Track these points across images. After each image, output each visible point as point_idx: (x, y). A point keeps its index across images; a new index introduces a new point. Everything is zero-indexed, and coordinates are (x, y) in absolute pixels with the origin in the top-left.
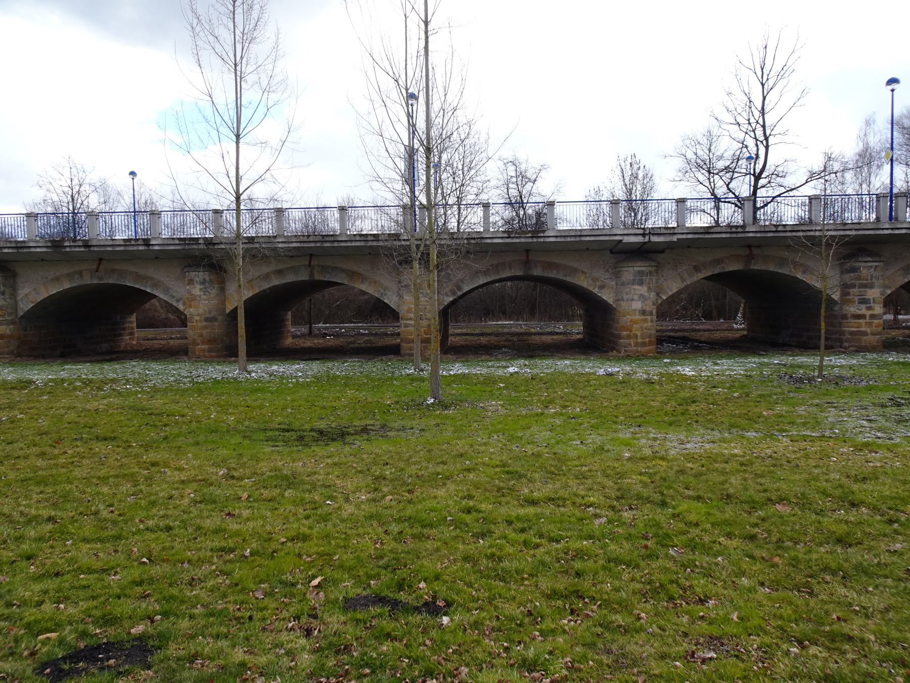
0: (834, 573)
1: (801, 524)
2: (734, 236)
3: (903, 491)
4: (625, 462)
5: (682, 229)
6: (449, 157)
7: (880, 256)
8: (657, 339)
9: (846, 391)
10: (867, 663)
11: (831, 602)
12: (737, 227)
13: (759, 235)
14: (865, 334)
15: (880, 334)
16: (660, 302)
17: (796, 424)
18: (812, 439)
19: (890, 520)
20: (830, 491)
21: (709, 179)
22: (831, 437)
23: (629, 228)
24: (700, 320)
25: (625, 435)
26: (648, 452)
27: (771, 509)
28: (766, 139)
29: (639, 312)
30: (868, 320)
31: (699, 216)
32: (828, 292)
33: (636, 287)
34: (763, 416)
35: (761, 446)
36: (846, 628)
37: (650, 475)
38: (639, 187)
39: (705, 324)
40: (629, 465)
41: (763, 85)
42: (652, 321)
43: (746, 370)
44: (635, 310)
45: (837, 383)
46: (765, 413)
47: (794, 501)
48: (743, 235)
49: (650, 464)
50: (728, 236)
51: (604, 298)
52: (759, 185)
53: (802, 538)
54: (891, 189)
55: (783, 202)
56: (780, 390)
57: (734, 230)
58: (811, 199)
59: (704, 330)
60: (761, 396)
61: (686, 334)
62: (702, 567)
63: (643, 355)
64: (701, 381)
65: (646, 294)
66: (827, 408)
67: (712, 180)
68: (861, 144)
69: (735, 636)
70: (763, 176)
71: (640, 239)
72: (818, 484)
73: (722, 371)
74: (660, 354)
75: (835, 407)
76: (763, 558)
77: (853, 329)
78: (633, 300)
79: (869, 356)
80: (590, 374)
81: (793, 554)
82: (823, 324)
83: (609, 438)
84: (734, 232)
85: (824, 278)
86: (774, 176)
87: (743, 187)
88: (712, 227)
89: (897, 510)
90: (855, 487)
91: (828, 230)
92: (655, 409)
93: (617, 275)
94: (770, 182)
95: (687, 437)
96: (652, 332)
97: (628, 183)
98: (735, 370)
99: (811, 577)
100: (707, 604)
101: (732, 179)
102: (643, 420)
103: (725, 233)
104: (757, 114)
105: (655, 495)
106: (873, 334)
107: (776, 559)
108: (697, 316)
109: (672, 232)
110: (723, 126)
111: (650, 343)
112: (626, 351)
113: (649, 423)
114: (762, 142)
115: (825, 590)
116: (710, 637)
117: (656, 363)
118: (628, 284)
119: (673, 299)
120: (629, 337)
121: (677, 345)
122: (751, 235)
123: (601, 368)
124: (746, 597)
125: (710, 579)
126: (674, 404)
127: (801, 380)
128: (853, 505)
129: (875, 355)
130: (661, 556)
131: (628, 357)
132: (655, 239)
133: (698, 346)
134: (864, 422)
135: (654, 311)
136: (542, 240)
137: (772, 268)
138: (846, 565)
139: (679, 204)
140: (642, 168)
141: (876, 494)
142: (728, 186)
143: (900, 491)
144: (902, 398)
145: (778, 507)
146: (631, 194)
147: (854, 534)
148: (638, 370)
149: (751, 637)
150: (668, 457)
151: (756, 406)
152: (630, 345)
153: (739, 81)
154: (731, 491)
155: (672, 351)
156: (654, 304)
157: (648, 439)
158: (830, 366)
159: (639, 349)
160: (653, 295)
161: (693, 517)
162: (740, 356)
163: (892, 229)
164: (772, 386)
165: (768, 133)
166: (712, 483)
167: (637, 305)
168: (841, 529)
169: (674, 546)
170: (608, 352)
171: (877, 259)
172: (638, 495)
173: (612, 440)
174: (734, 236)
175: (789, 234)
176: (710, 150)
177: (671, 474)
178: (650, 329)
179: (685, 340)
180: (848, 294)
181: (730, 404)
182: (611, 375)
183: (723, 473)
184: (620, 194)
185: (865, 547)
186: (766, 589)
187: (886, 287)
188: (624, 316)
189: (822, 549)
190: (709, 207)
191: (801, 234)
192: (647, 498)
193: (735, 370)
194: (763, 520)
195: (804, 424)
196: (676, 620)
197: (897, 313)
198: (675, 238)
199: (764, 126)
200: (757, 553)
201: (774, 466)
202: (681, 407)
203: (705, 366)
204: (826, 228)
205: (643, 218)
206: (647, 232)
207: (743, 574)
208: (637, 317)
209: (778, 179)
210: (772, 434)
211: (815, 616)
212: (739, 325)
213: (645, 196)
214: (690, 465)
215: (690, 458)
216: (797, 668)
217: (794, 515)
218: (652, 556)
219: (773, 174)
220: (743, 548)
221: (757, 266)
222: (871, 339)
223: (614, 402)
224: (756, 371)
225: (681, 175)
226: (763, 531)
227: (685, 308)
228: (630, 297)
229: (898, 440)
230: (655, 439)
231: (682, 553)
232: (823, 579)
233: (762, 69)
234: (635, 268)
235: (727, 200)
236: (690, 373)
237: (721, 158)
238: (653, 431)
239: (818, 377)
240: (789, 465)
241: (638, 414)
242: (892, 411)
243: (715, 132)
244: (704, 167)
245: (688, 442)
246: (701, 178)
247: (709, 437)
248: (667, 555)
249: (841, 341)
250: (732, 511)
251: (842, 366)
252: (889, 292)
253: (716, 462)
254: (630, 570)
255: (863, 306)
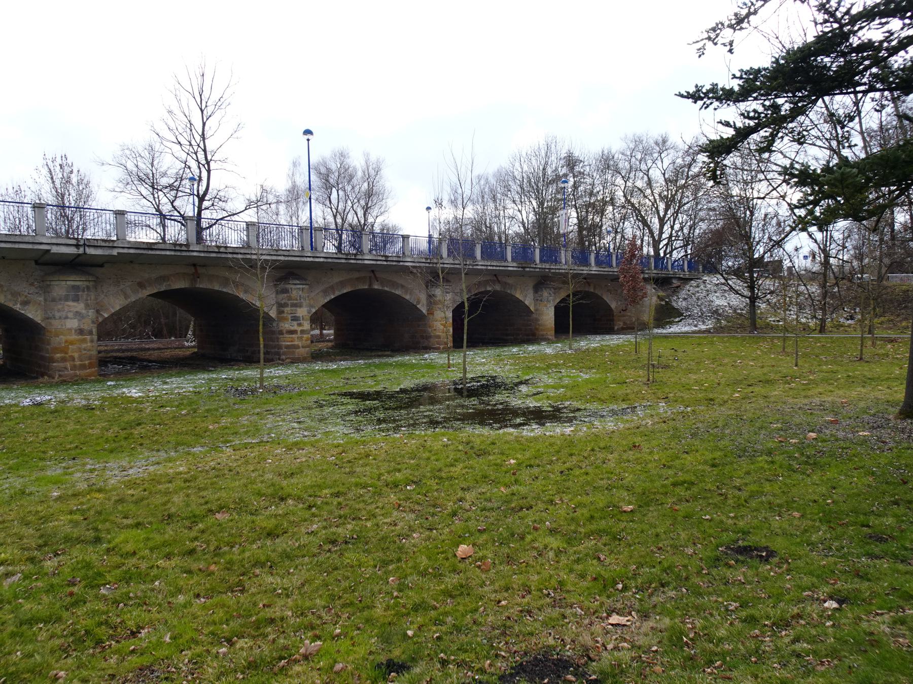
0: (263, 565)
1: (237, 527)
2: (179, 254)
3: (321, 479)
4: (51, 503)
5: (122, 243)
6: (339, 166)
7: (305, 280)
8: (100, 361)
9: (282, 398)
10: (285, 638)
11: (259, 593)
12: (181, 245)
13: (202, 255)
14: (297, 347)
15: (308, 346)
16: (100, 320)
17: (240, 434)
18: (251, 445)
19: (310, 506)
20: (264, 491)
21: (153, 194)
22: (268, 442)
23: (60, 237)
24: (149, 338)
25: (55, 471)
26: (82, 486)
27: (210, 520)
28: (208, 163)
29: (76, 331)
30: (299, 335)
31: (144, 231)
32: (266, 309)
33: (71, 303)
34: (209, 430)
35: (207, 459)
36: (269, 613)
37: (83, 512)
38: (73, 193)
39: (155, 343)
40: (57, 506)
41: (202, 111)
42: (92, 341)
43: (195, 387)
44: (70, 329)
45: (275, 392)
46: (211, 427)
47: (233, 506)
48: (188, 254)
49: (84, 500)
50: (173, 253)
51: (30, 315)
52: (203, 207)
53: (237, 540)
54: (311, 223)
55: (227, 225)
56: (225, 403)
57: (178, 248)
58: (248, 224)
59: (154, 349)
60: (208, 411)
61: (135, 354)
62: (136, 597)
63: (82, 379)
64: (148, 401)
65: (84, 311)
66: (266, 415)
67: (156, 196)
68: (290, 182)
69: (167, 658)
70: (206, 198)
71: (72, 250)
72: (254, 486)
73: (172, 389)
74: (103, 377)
75: (272, 414)
76: (200, 570)
77: (289, 343)
78: (67, 318)
79: (301, 366)
80: (11, 406)
81: (228, 557)
82: (261, 339)
83: (33, 478)
84: (178, 250)
85: (260, 298)
86: (217, 200)
87: (187, 207)
88: (159, 243)
89: (316, 496)
90: (284, 483)
91: (262, 254)
92: (94, 437)
93: (45, 289)
94: (213, 205)
95: (129, 463)
96: (92, 353)
97: (58, 186)
98: (185, 388)
99: (243, 575)
100: (139, 635)
101: (176, 197)
102: (78, 451)
103: (310, 257)
104: (198, 138)
105: (88, 533)
106: (303, 347)
107: (213, 567)
108: (147, 334)
109: (111, 245)
110: (164, 142)
111: (91, 366)
112: (60, 376)
113: (86, 454)
114: (204, 165)
115: (255, 583)
116: (140, 670)
117: (98, 386)
118: (60, 300)
119: (117, 317)
120: (64, 360)
121: (124, 366)
122: (195, 254)
123: (26, 398)
124: (181, 614)
125: (145, 607)
126: (116, 429)
127: (244, 392)
128: (282, 499)
129: (305, 365)
130: (89, 599)
131: (64, 382)
132: (91, 251)
133: (147, 366)
134: (295, 424)
135: (94, 331)
136: (401, 263)
137: (217, 287)
138: (273, 555)
139: (118, 216)
140: (75, 171)
141: (299, 487)
142: (172, 203)
143: (318, 480)
144: (324, 400)
145: (218, 516)
146: (63, 198)
147: (281, 525)
148: (75, 396)
149: (183, 653)
150: (107, 488)
151: (203, 421)
152: (66, 368)
153: (179, 101)
154: (173, 510)
155: (117, 373)
156: (93, 322)
157: (84, 472)
158: (270, 377)
159: (78, 372)
160: (91, 313)
161: (130, 547)
162: (190, 373)
163: (313, 257)
164: (219, 400)
165: (209, 158)
166: (153, 506)
167: (73, 324)
168: (270, 524)
169: (107, 584)
170: (37, 378)
171: (304, 282)
172: (65, 538)
173: (37, 480)
174: (179, 254)
175: (230, 256)
176: (152, 165)
177: (109, 505)
178: (89, 350)
179: (132, 360)
180: (283, 312)
181: (177, 422)
182: (40, 404)
183: (167, 493)
184: (48, 197)
185: (290, 534)
186: (202, 599)
187: (311, 306)
188: (57, 335)
189: (255, 546)
190: (155, 224)
191: (240, 256)
192: (77, 539)
193: (185, 388)
194: (203, 532)
195: (246, 433)
196: (104, 664)
197: (322, 329)
198: (115, 252)
199: (205, 151)
200: (195, 566)
201: (217, 476)
202: (125, 431)
203: (153, 385)
204: (260, 252)
205: (81, 227)
206: (82, 243)
207: (180, 591)
208: (74, 337)
209: (221, 203)
210: (217, 447)
211: (244, 610)
212: (190, 343)
213: (81, 205)
214: (130, 492)
215: (132, 484)
216: (225, 666)
217: (232, 520)
218: (79, 602)
219: (215, 198)
220: (181, 565)
221: (203, 285)
222: (302, 352)
223: (42, 436)
224: (205, 387)
225: (122, 187)
226: (202, 542)
227: (133, 326)
228: (64, 314)
229: (320, 436)
230: (92, 471)
231: (116, 588)
232: (253, 573)
233: (201, 95)
234: (68, 283)
235: (172, 218)
236: (137, 395)
237: (164, 174)
238: (91, 462)
239: (260, 388)
240: (231, 473)
241: (73, 445)
242: (316, 412)
243: (157, 147)
244: (147, 181)
245: (131, 468)
246: (145, 192)
247: (154, 459)
248: (96, 597)
249: (278, 354)
250: (173, 531)
251: (279, 377)
252: (314, 310)
253: (159, 483)
254: (49, 626)
255: (295, 323)
